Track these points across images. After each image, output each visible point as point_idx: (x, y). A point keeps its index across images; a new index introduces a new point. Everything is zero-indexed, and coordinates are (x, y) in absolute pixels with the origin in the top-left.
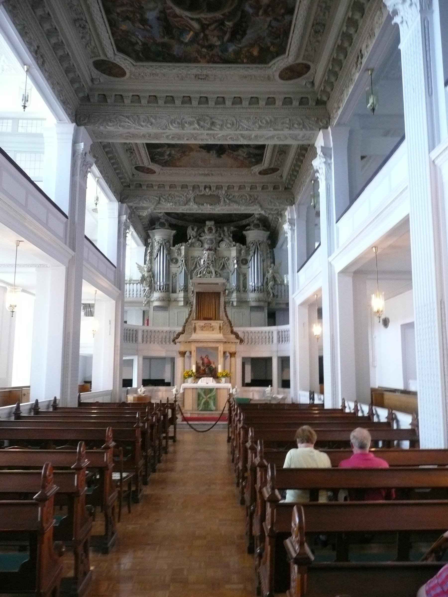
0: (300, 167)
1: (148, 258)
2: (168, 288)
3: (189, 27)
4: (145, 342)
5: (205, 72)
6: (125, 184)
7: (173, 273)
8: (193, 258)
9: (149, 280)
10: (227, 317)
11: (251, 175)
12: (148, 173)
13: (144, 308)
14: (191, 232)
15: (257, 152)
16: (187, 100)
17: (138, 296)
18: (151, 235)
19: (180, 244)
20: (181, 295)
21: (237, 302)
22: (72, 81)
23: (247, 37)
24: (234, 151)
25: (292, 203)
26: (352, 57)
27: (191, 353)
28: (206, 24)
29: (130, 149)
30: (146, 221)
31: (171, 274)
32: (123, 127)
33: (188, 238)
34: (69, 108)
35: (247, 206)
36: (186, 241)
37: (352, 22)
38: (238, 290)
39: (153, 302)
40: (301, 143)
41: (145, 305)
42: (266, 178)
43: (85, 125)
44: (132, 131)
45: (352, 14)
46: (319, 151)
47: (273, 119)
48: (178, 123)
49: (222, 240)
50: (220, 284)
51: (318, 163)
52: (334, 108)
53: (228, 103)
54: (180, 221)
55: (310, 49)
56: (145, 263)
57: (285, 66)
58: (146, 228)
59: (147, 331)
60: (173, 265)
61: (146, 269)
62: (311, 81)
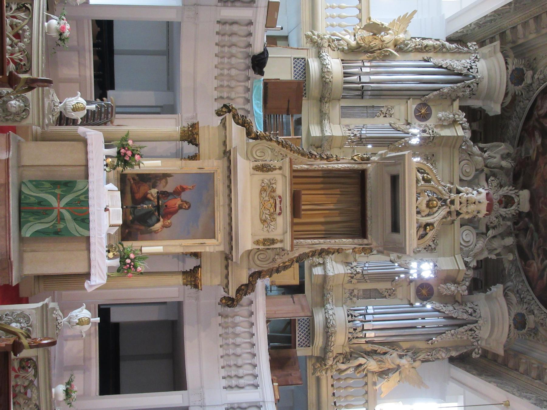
4: (218, 28)
7: (392, 108)
14: (498, 153)
18: (486, 50)
19: (467, 125)
27: (194, 157)
33: (481, 145)
36: (475, 138)
39: (319, 56)
41: (307, 37)
60: (414, 106)
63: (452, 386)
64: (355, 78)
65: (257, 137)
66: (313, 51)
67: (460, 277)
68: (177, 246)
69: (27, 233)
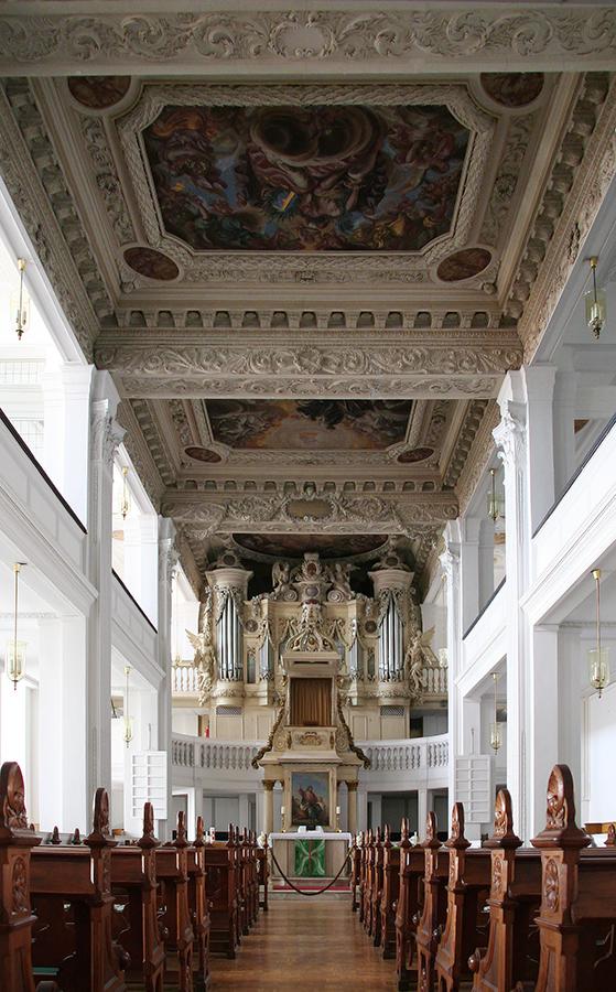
0: (469, 445)
1: (206, 621)
2: (242, 674)
3: (288, 185)
5: (312, 266)
6: (168, 482)
8: (283, 621)
9: (209, 661)
10: (343, 721)
11: (384, 464)
12: (206, 461)
13: (200, 711)
14: (279, 574)
15: (397, 417)
16: (281, 319)
17: (191, 688)
18: (210, 580)
19: (261, 596)
20: (264, 686)
21: (358, 697)
22: (89, 290)
23: (384, 201)
24: (357, 416)
25: (455, 515)
26: (561, 238)
28: (317, 178)
29: (179, 414)
30: (202, 554)
31: (246, 650)
32: (173, 369)
34: (85, 339)
35: (379, 519)
36: (270, 589)
37: (562, 173)
38: (360, 679)
40: (473, 396)
42: (409, 469)
43: (108, 367)
44: (188, 375)
45: (563, 159)
46: (504, 412)
47: (426, 353)
48: (266, 361)
49: (332, 588)
50: (331, 663)
51: (502, 433)
52: (531, 332)
53: (351, 323)
54: (259, 555)
55: (491, 221)
56: (200, 630)
57: (448, 254)
58: (202, 561)
59: (209, 747)
61: (202, 641)
62: (492, 282)
63: (439, 602)
64: (230, 673)
65: (271, 745)
66: (212, 701)
67: (362, 603)
68: (333, 795)
69: (322, 872)
